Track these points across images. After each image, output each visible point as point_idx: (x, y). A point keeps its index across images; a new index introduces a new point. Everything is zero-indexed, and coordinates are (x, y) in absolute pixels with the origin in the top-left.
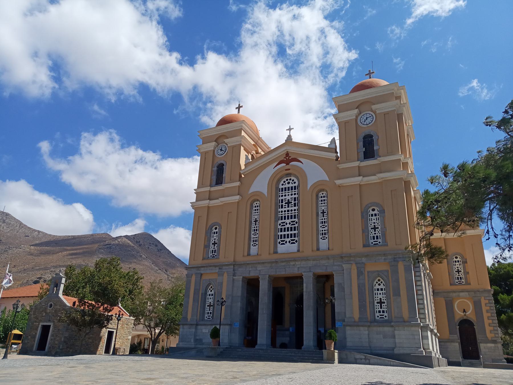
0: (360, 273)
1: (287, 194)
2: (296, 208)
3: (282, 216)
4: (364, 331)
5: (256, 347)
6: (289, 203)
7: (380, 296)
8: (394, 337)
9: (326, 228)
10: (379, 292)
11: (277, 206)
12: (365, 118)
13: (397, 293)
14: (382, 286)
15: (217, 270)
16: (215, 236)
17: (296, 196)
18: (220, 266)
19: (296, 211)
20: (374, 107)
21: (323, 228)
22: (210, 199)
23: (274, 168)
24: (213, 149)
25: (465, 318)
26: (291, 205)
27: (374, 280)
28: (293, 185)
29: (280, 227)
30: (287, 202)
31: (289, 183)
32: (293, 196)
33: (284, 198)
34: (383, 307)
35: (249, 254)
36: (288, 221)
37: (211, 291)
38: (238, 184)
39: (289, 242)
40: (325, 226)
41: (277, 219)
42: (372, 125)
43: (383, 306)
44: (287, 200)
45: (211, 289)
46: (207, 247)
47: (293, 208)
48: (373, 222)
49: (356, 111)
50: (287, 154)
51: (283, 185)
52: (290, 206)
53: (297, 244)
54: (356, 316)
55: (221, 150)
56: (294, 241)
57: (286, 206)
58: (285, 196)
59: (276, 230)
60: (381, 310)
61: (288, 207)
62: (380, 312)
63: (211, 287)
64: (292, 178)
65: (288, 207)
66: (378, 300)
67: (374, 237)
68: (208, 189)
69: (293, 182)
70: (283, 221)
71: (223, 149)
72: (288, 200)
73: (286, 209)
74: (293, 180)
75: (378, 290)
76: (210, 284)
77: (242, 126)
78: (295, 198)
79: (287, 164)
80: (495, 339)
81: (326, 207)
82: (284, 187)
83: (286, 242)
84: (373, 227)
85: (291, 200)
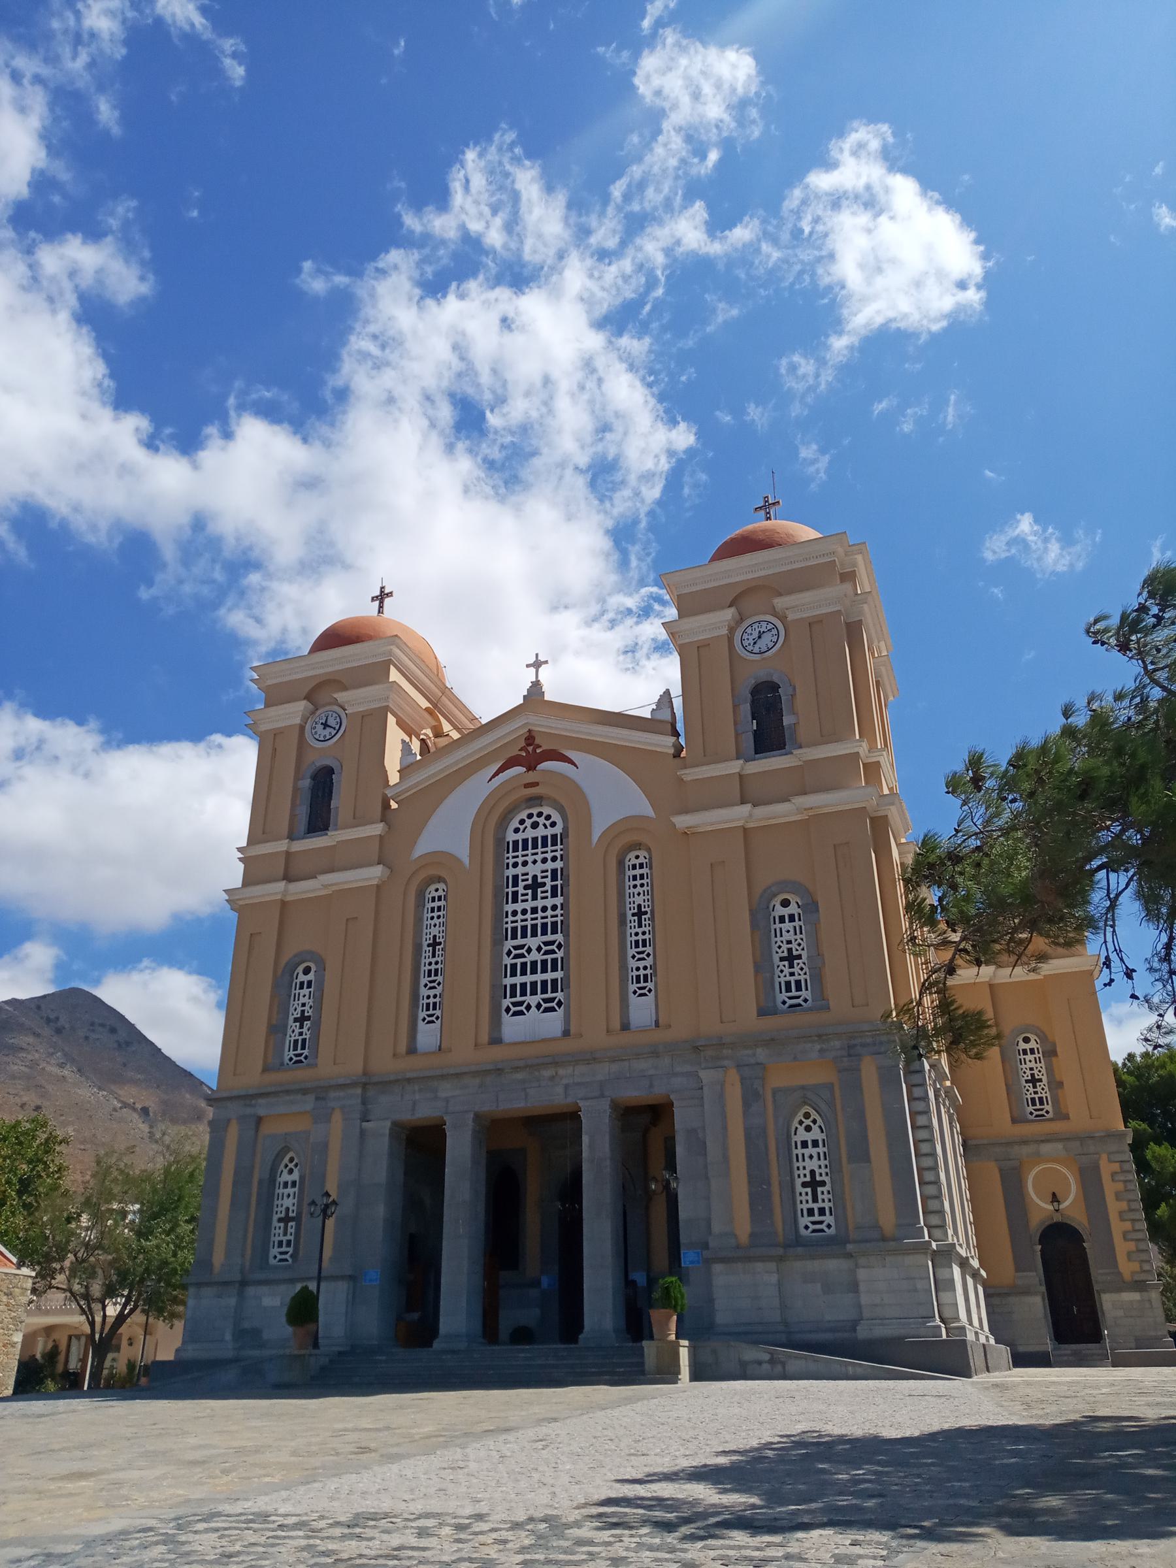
0: (751, 1097)
1: (530, 859)
2: (558, 901)
3: (517, 927)
4: (766, 1275)
5: (437, 1345)
6: (535, 885)
7: (811, 1163)
8: (854, 1287)
9: (649, 962)
10: (807, 1152)
11: (500, 898)
12: (756, 635)
13: (861, 1154)
14: (816, 1134)
15: (309, 1103)
16: (304, 996)
17: (558, 864)
18: (321, 1092)
19: (559, 912)
20: (780, 603)
21: (639, 959)
22: (288, 878)
23: (490, 780)
24: (298, 721)
25: (1057, 1218)
26: (542, 892)
27: (793, 1114)
28: (549, 832)
29: (508, 961)
30: (530, 882)
31: (535, 825)
32: (550, 865)
33: (520, 870)
34: (820, 1197)
35: (412, 1050)
36: (533, 942)
37: (291, 1172)
38: (377, 829)
39: (539, 1006)
40: (644, 956)
41: (500, 936)
42: (775, 655)
43: (819, 1193)
44: (530, 877)
45: (291, 1166)
46: (277, 1029)
47: (549, 903)
48: (784, 939)
49: (729, 614)
50: (530, 738)
51: (517, 831)
52: (540, 895)
53: (560, 1011)
54: (743, 1227)
55: (326, 725)
56: (554, 1004)
57: (527, 894)
58: (525, 864)
59: (498, 970)
60: (815, 1206)
61: (535, 898)
62: (811, 1212)
63: (291, 1160)
64: (546, 810)
65: (535, 898)
66: (805, 1176)
67: (788, 984)
68: (282, 846)
69: (548, 823)
70: (519, 941)
71: (331, 722)
72: (535, 877)
73: (528, 906)
74: (548, 817)
75: (804, 1144)
76: (286, 1150)
77: (390, 653)
78: (554, 872)
79: (531, 768)
80: (1142, 1277)
81: (646, 897)
82: (520, 837)
83: (529, 1007)
84: (785, 954)
85: (543, 877)
